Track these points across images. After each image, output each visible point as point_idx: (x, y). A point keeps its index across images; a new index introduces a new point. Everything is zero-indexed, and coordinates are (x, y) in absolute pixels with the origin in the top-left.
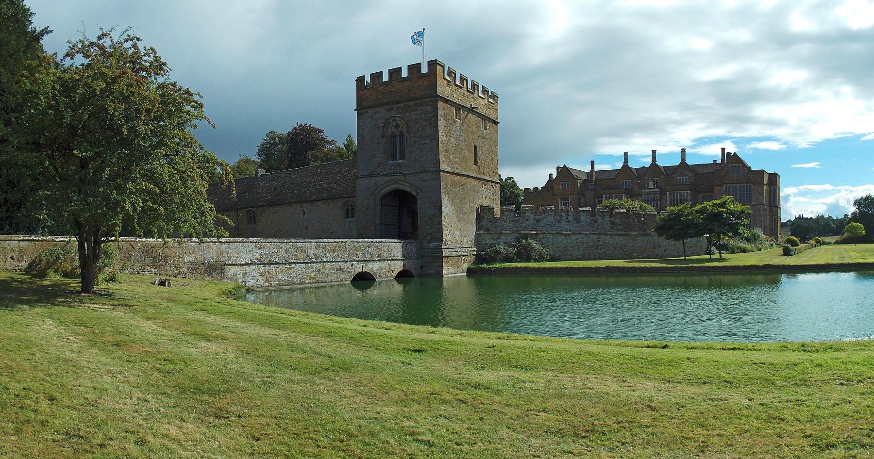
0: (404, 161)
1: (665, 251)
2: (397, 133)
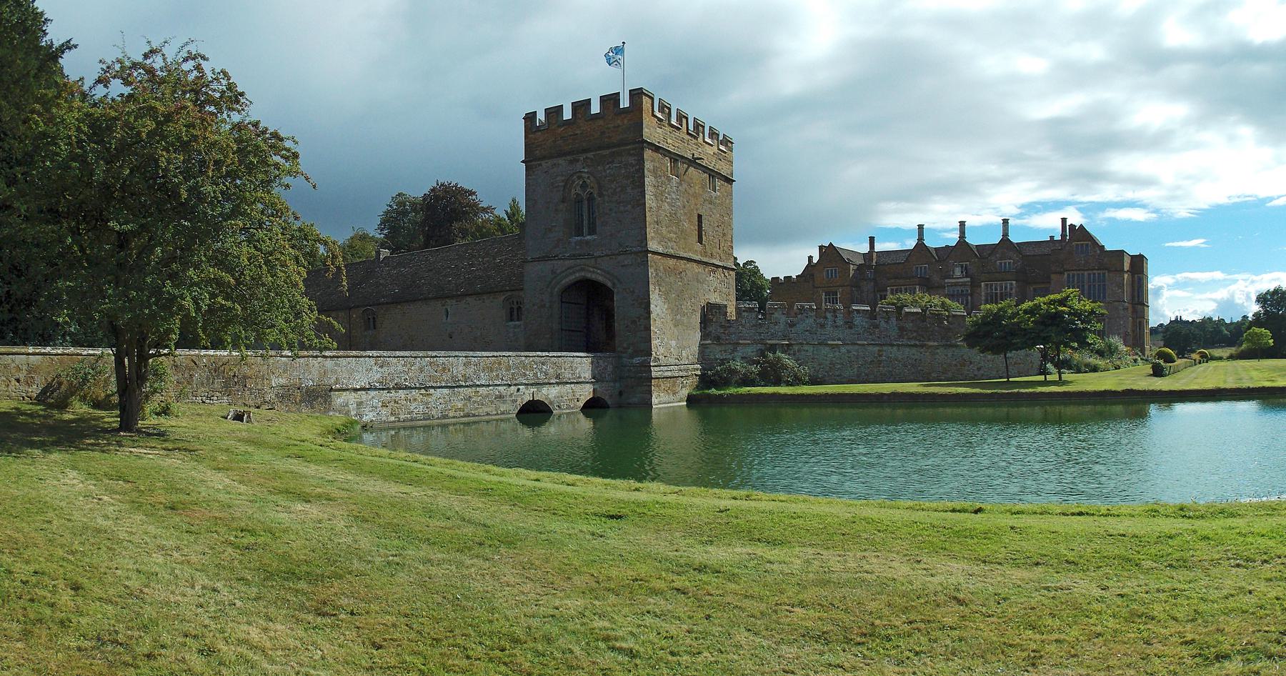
0: (595, 237)
1: (979, 369)
2: (585, 196)
